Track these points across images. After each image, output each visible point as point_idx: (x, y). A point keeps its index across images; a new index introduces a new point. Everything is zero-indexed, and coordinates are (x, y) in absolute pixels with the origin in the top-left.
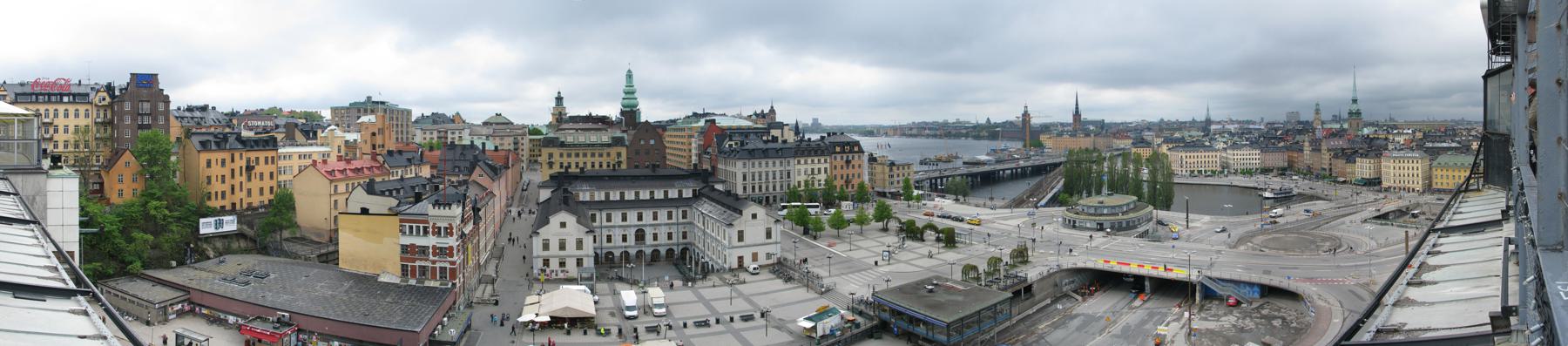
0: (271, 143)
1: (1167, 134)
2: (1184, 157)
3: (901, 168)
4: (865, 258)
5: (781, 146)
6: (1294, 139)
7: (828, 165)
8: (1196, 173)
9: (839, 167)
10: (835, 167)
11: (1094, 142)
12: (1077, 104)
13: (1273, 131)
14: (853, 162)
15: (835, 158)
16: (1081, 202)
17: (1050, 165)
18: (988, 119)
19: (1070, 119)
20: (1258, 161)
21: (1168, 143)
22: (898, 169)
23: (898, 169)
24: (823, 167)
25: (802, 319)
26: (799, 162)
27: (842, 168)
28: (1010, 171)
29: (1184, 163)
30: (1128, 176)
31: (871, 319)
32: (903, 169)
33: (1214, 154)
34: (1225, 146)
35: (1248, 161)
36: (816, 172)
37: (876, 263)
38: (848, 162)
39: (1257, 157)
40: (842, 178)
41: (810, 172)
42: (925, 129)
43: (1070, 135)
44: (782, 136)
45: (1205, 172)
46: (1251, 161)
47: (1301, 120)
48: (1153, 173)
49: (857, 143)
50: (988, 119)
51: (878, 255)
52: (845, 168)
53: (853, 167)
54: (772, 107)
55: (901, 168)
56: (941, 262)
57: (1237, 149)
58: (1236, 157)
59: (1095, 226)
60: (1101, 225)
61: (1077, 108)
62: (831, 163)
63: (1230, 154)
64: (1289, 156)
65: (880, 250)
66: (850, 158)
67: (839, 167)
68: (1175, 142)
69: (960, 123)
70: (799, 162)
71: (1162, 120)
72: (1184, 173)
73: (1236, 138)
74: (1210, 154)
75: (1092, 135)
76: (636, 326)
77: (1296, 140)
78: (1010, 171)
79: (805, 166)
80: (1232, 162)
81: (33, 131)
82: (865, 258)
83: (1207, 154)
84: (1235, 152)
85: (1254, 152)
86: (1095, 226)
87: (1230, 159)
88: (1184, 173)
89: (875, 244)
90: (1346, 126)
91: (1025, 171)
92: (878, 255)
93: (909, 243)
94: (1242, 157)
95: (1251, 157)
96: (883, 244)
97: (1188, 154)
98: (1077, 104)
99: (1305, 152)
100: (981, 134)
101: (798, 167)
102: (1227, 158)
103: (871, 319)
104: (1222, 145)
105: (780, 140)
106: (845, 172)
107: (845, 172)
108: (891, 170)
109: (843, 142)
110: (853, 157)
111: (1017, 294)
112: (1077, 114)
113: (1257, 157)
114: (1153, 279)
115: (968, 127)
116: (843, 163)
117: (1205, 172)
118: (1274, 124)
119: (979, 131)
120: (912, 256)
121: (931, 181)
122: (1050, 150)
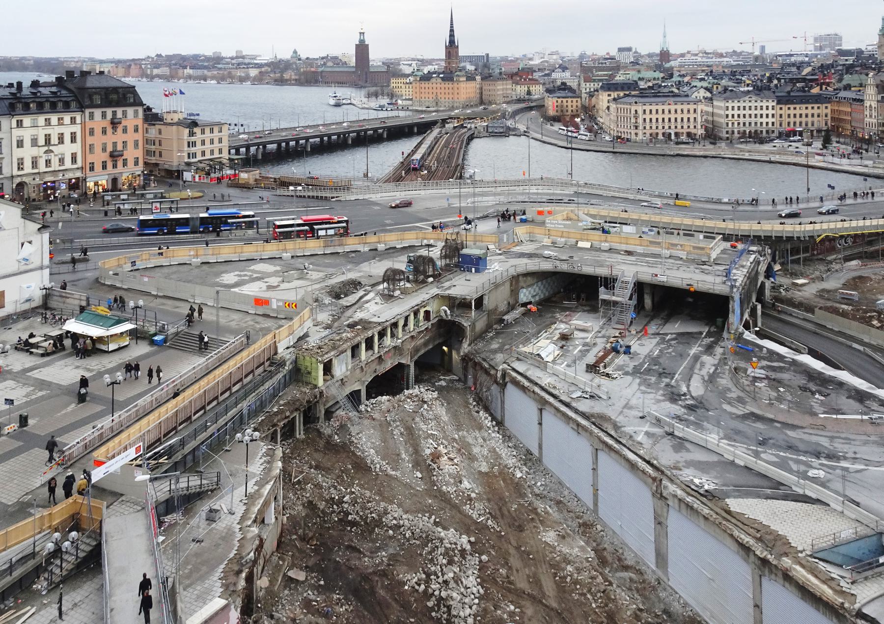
0: (213, 514)
2: (640, 112)
3: (207, 130)
6: (840, 80)
7: (77, 129)
8: (660, 137)
9: (98, 131)
10: (92, 132)
11: (481, 89)
12: (452, 31)
13: (794, 69)
14: (124, 123)
15: (92, 116)
17: (418, 125)
18: (295, 52)
19: (440, 53)
20: (770, 120)
21: (609, 90)
22: (203, 132)
23: (203, 132)
24: (67, 131)
26: (20, 124)
27: (104, 131)
28: (274, 146)
29: (640, 121)
32: (212, 131)
33: (692, 107)
34: (708, 95)
35: (753, 120)
36: (54, 140)
38: (114, 123)
39: (770, 112)
40: (104, 150)
41: (41, 141)
42: (185, 67)
43: (443, 79)
45: (677, 135)
46: (759, 120)
47: (845, 47)
49: (131, 89)
50: (295, 52)
52: (109, 130)
53: (125, 131)
55: (207, 130)
57: (733, 99)
58: (730, 112)
61: (452, 35)
62: (84, 124)
63: (719, 108)
64: (833, 111)
66: (119, 115)
67: (98, 131)
68: (623, 89)
69: (243, 57)
70: (20, 124)
71: (582, 56)
72: (640, 136)
73: (724, 82)
74: (685, 107)
75: (478, 78)
76: (83, 467)
77: (844, 82)
78: (274, 146)
79: (33, 131)
80: (723, 121)
81: (681, 366)
83: (679, 107)
84: (730, 104)
85: (764, 104)
87: (720, 116)
88: (640, 136)
90: (767, 75)
91: (346, 139)
94: (742, 112)
95: (759, 112)
98: (452, 31)
99: (867, 104)
100: (286, 76)
101: (17, 133)
102: (713, 114)
104: (703, 93)
106: (110, 138)
107: (119, 137)
108: (192, 134)
109: (106, 89)
110: (125, 114)
112: (452, 46)
113: (770, 112)
114: (848, 318)
115: (259, 66)
116: (106, 123)
117: (677, 135)
118: (792, 55)
119: (282, 72)
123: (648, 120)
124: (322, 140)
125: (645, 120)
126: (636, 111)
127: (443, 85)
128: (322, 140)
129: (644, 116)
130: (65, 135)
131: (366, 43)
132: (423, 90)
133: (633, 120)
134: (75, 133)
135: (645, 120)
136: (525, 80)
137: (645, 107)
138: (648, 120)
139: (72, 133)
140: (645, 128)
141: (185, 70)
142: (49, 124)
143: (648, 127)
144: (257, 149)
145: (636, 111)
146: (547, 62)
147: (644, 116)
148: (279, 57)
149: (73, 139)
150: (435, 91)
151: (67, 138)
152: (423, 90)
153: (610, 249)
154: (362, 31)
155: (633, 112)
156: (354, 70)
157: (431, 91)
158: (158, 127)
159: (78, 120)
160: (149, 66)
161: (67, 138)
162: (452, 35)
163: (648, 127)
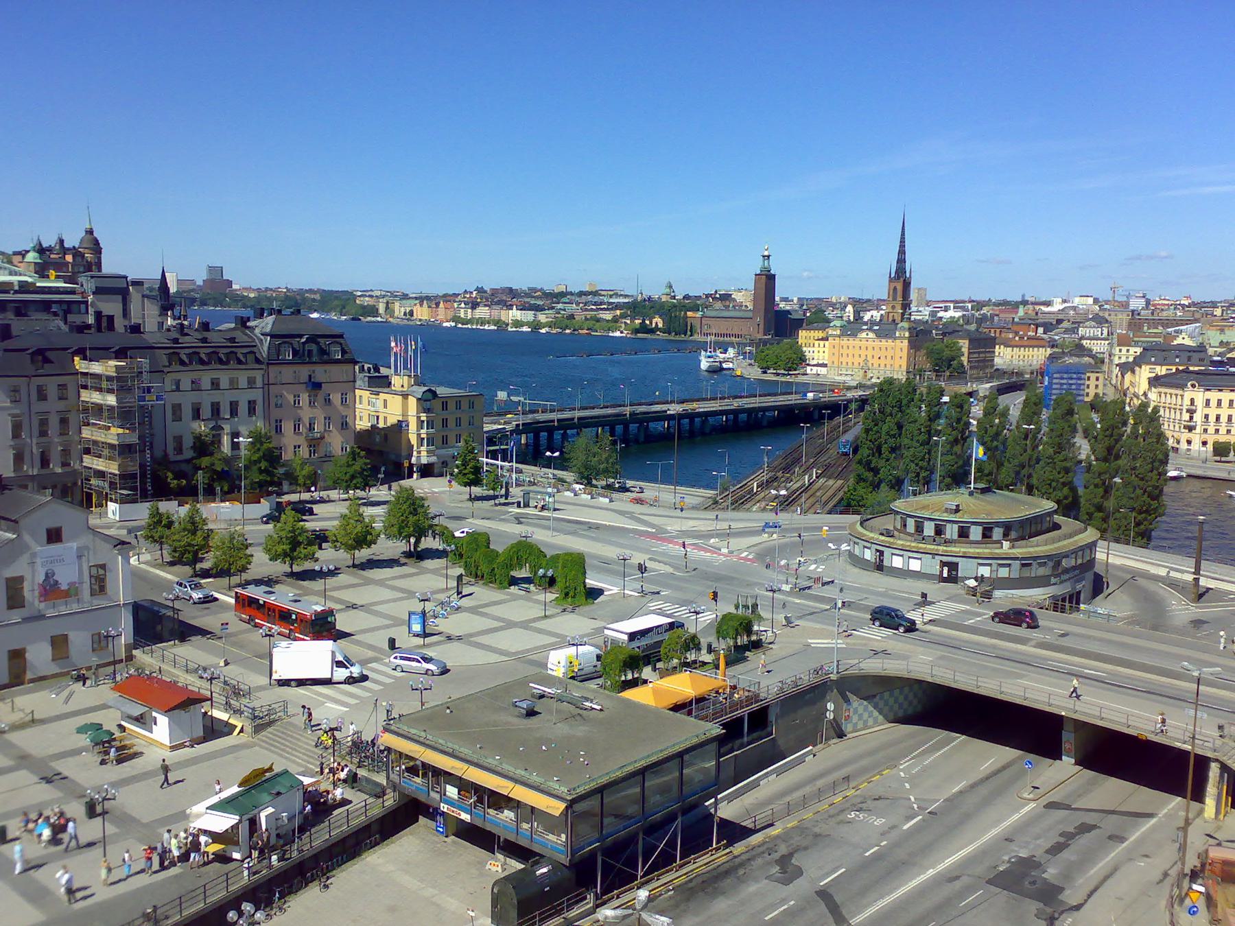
1: (1154, 334)
2: (1199, 403)
4: (394, 600)
5: (1061, 307)
7: (257, 395)
12: (902, 251)
16: (898, 505)
24: (243, 398)
25: (200, 808)
29: (1198, 417)
30: (968, 424)
31: (380, 794)
37: (392, 643)
41: (206, 412)
44: (126, 313)
48: (987, 413)
51: (397, 622)
54: (90, 232)
56: (554, 640)
59: (936, 570)
60: (953, 567)
61: (901, 261)
65: (401, 609)
82: (394, 600)
86: (936, 570)
88: (1196, 445)
89: (387, 594)
92: (397, 622)
93: (481, 593)
96: (410, 594)
97: (1214, 396)
103: (380, 794)
105: (119, 324)
111: (733, 730)
120: (479, 623)
121: (537, 437)
122: (823, 371)
123: (1212, 419)
124: (736, 418)
125: (1207, 416)
126: (1192, 401)
127: (877, 343)
128: (736, 418)
129: (1207, 411)
130: (240, 404)
131: (772, 272)
132: (845, 352)
133: (1186, 416)
134: (254, 402)
135: (1207, 416)
136: (1021, 338)
137: (1209, 395)
138: (1212, 419)
139: (249, 402)
140: (1205, 431)
141: (510, 311)
142: (178, 389)
143: (1211, 430)
144: (638, 428)
145: (1192, 401)
146: (1074, 308)
147: (1207, 411)
148: (646, 294)
149: (252, 410)
150: (863, 353)
151: (243, 408)
152: (845, 352)
153: (33, 721)
154: (766, 253)
155: (1187, 402)
156: (750, 315)
157: (857, 352)
158: (382, 396)
159: (259, 383)
160: (463, 305)
161: (243, 408)
162: (901, 261)
163: (1211, 430)
